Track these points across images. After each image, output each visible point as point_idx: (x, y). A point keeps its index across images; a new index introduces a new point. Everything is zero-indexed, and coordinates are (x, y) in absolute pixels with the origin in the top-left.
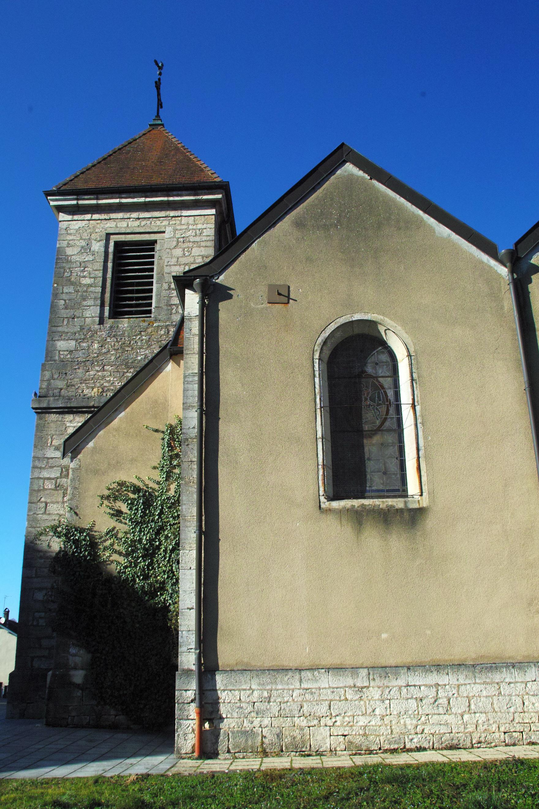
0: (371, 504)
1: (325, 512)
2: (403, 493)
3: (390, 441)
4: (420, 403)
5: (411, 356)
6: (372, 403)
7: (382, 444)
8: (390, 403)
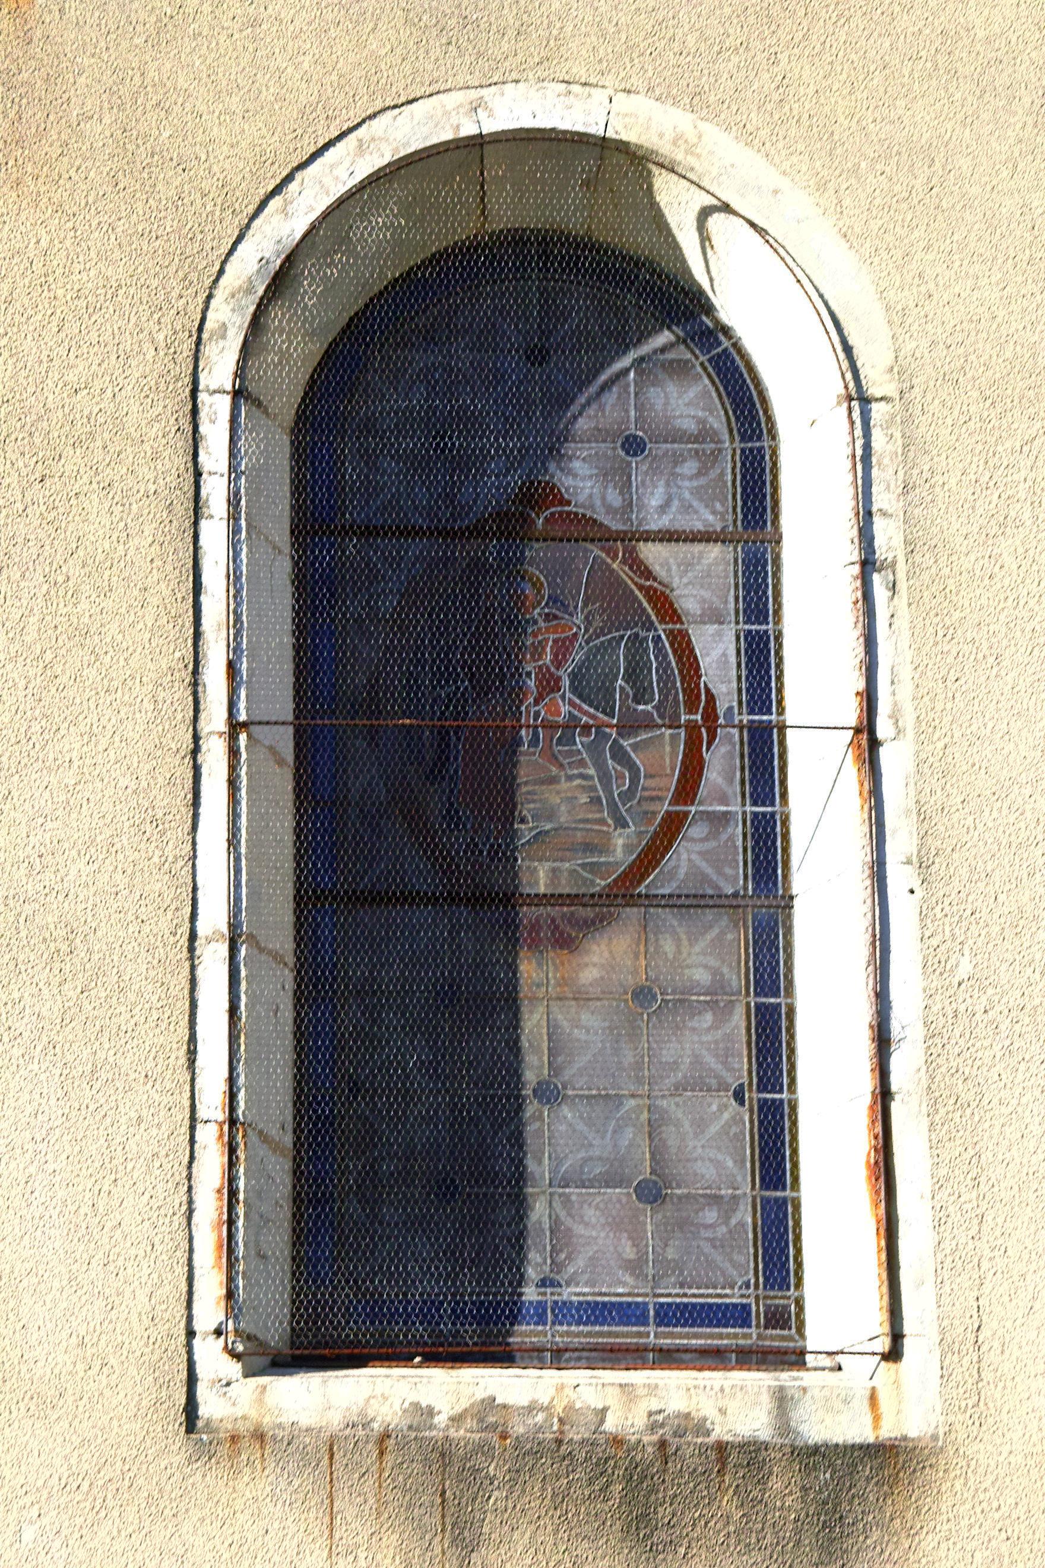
0: (545, 1400)
1: (224, 1450)
2: (774, 1339)
3: (702, 976)
4: (908, 720)
5: (865, 401)
6: (587, 714)
7: (642, 994)
8: (710, 714)
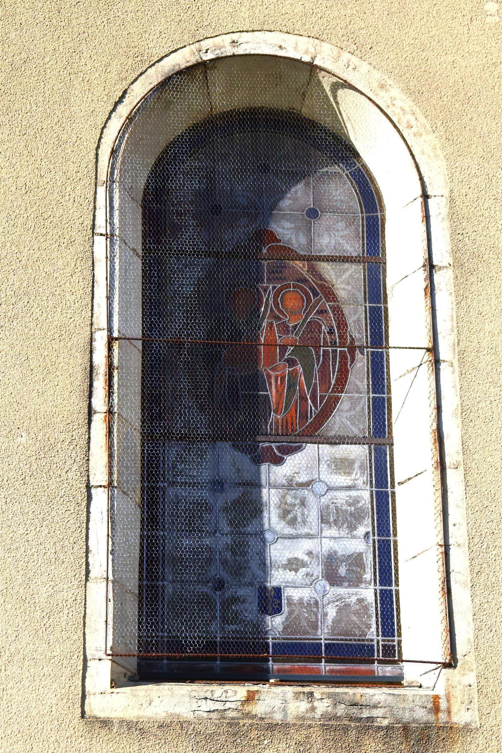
2: (388, 670)
